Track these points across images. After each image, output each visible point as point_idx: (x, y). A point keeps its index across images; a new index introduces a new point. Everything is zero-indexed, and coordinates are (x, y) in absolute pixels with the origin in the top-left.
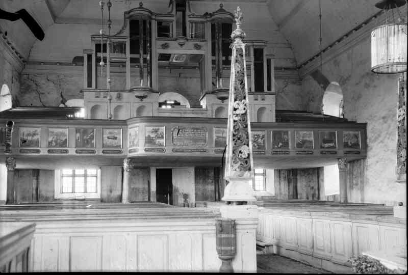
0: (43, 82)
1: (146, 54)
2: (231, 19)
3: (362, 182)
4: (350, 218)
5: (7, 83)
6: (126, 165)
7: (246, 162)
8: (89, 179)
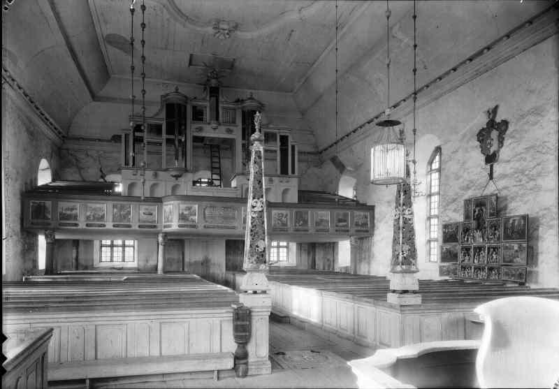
0: (83, 156)
3: (369, 256)
4: (353, 299)
5: (46, 158)
6: (160, 239)
7: (262, 256)
8: (127, 249)
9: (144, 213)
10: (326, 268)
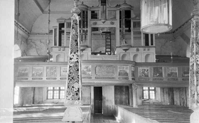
0: (39, 43)
1: (84, 28)
2: (130, 8)
7: (77, 94)
9: (63, 71)
10: (182, 104)
